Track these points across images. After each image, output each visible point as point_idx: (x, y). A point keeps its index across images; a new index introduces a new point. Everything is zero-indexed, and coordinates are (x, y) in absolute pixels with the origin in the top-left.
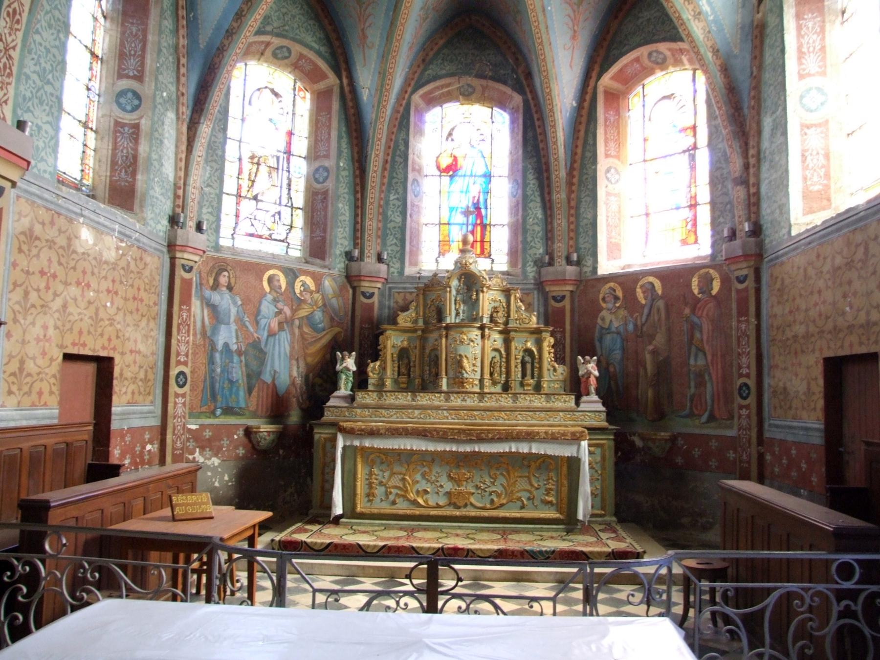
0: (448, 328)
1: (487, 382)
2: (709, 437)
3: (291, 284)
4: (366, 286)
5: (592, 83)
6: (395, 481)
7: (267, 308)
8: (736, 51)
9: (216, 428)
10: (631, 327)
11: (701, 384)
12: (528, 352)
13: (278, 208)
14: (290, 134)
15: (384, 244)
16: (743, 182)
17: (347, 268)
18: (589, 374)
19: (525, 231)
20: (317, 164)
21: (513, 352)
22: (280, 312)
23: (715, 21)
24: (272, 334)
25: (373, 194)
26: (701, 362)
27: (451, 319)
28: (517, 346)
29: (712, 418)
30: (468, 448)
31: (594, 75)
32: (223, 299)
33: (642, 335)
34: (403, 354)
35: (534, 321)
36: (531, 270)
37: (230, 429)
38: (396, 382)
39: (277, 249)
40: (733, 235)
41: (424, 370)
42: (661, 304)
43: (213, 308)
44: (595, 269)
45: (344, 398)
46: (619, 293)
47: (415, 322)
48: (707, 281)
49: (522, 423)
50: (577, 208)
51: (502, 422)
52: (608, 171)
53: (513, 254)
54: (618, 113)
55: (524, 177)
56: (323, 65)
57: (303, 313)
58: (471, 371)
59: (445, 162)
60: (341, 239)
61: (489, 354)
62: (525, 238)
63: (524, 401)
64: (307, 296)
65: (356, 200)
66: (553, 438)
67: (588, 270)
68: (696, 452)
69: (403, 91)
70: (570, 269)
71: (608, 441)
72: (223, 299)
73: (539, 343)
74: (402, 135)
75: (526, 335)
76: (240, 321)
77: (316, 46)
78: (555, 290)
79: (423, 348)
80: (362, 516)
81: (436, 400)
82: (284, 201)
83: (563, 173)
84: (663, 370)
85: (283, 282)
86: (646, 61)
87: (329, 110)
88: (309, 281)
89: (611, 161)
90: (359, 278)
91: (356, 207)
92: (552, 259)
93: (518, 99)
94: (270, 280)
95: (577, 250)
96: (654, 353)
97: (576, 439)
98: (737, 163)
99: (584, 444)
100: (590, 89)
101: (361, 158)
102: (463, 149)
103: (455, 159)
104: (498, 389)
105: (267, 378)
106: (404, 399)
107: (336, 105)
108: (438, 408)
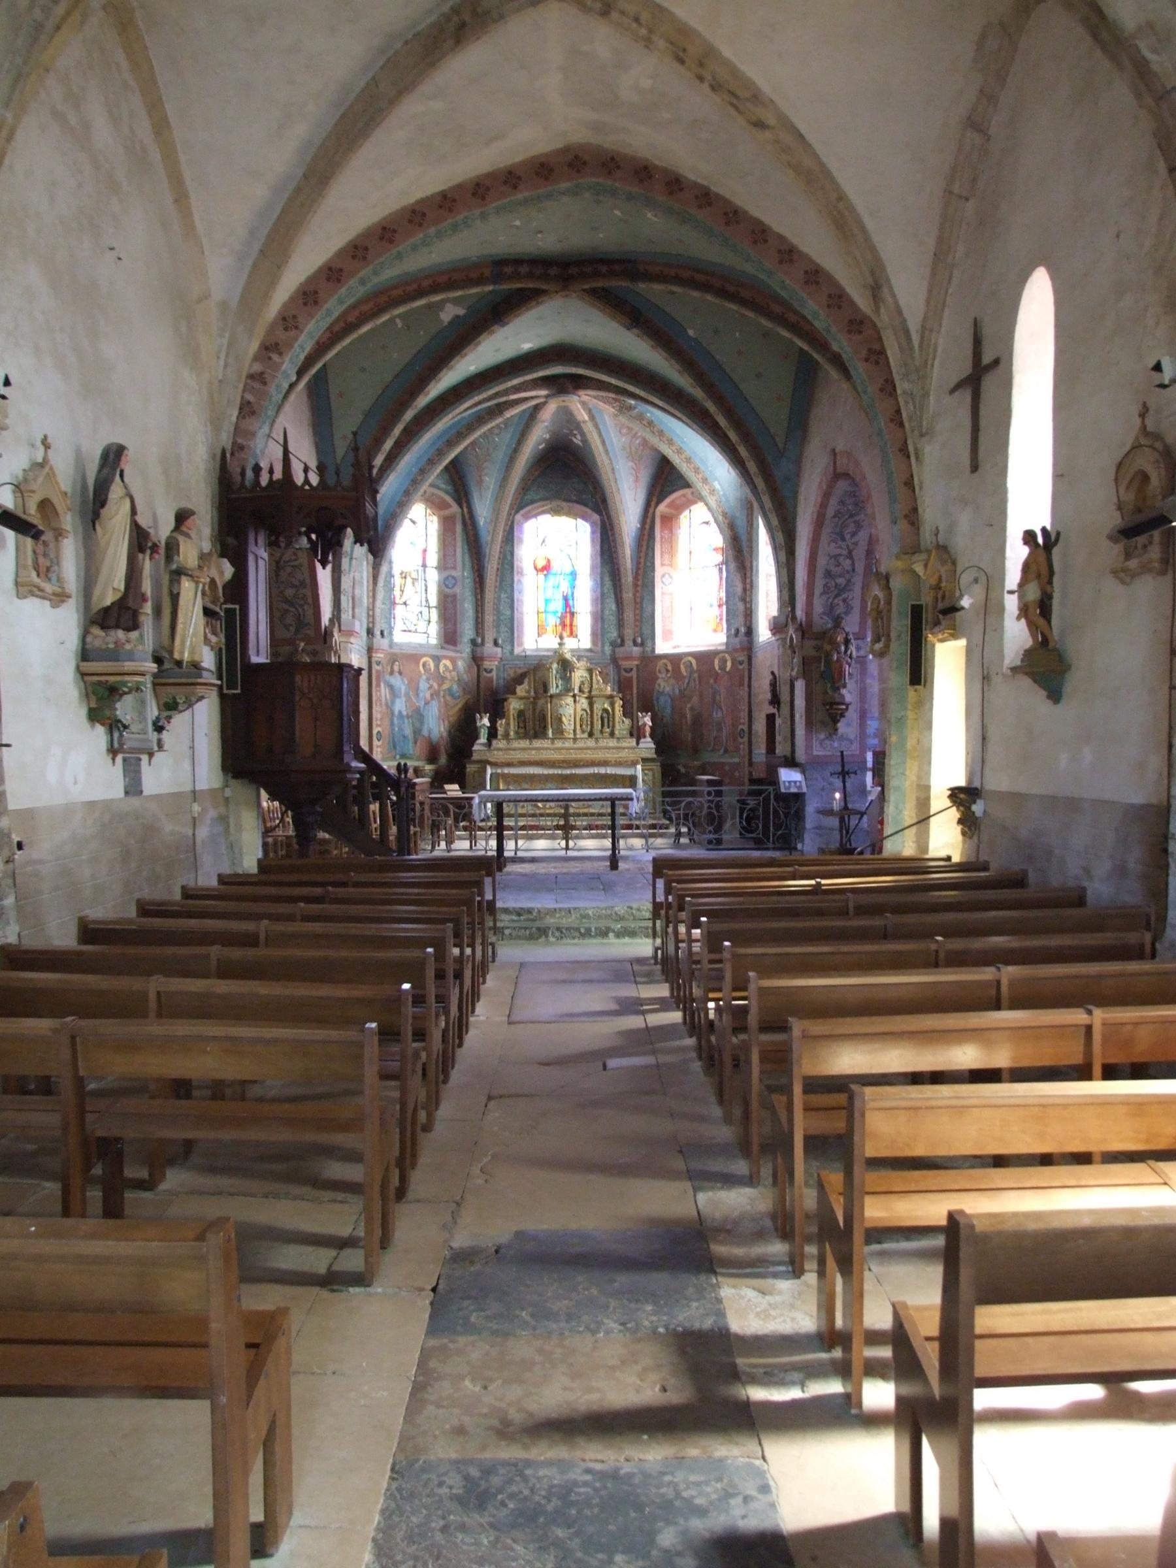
0: (551, 696)
1: (578, 731)
3: (437, 666)
4: (487, 664)
5: (651, 510)
7: (423, 685)
8: (738, 515)
10: (677, 691)
11: (720, 730)
12: (605, 710)
13: (420, 609)
14: (425, 551)
15: (498, 632)
16: (744, 600)
17: (473, 651)
18: (645, 724)
19: (603, 620)
20: (447, 573)
21: (595, 711)
22: (431, 687)
23: (724, 495)
24: (427, 703)
25: (489, 595)
26: (720, 715)
27: (553, 690)
28: (598, 707)
29: (726, 751)
30: (568, 772)
31: (653, 504)
32: (396, 681)
33: (684, 696)
34: (521, 714)
35: (609, 690)
36: (608, 649)
38: (517, 733)
39: (419, 639)
40: (737, 631)
41: (536, 724)
42: (696, 675)
43: (391, 687)
44: (653, 650)
45: (483, 744)
46: (670, 668)
47: (528, 692)
48: (724, 661)
49: (600, 755)
50: (641, 603)
51: (589, 756)
52: (663, 576)
53: (594, 634)
54: (671, 531)
55: (602, 578)
56: (448, 499)
57: (445, 687)
58: (568, 725)
59: (540, 565)
60: (467, 630)
61: (579, 712)
62: (603, 625)
63: (603, 743)
64: (448, 675)
65: (477, 600)
66: (619, 764)
67: (649, 649)
69: (509, 514)
70: (636, 649)
71: (656, 767)
72: (396, 681)
73: (612, 705)
74: (509, 548)
75: (603, 699)
77: (443, 486)
78: (625, 664)
79: (534, 710)
81: (545, 743)
82: (424, 603)
83: (630, 579)
84: (698, 720)
85: (432, 665)
86: (690, 497)
87: (454, 533)
88: (448, 663)
89: (666, 569)
90: (482, 659)
91: (477, 605)
92: (623, 641)
93: (596, 517)
94: (424, 665)
95: (641, 635)
96: (692, 709)
97: (634, 764)
98: (739, 588)
99: (639, 767)
100: (650, 515)
101: (480, 570)
102: (554, 551)
103: (549, 561)
104: (586, 735)
105: (425, 733)
106: (524, 743)
107: (459, 528)
108: (547, 749)
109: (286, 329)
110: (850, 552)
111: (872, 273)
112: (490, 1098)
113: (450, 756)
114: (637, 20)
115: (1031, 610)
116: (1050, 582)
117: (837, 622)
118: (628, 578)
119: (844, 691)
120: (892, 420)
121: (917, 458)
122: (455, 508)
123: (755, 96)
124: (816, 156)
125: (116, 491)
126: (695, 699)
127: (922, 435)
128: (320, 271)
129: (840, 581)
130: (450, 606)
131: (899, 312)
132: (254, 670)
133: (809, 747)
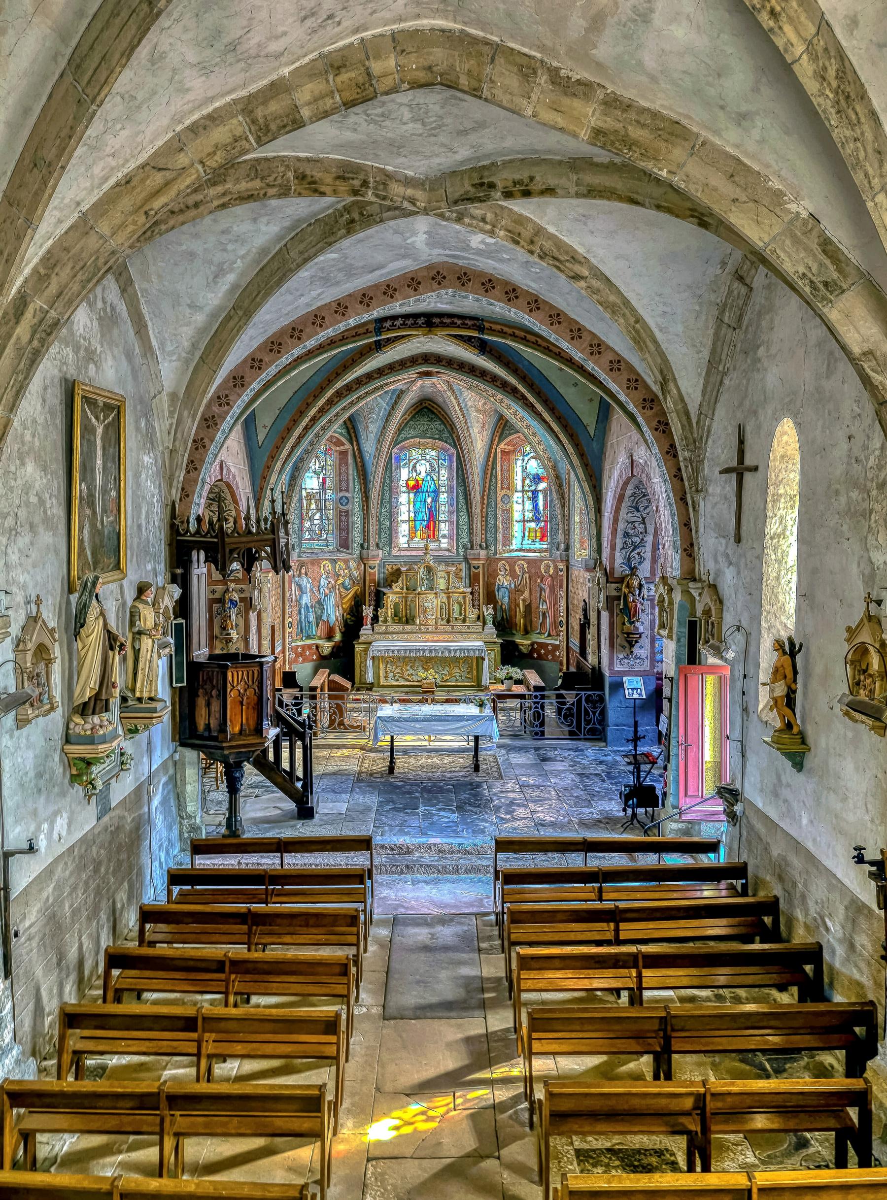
2: (548, 644)
3: (334, 568)
4: (371, 563)
6: (398, 670)
9: (303, 647)
12: (459, 603)
25: (373, 511)
29: (549, 635)
34: (396, 605)
37: (309, 647)
43: (300, 586)
57: (339, 582)
59: (412, 483)
68: (543, 652)
72: (305, 582)
76: (311, 590)
78: (474, 563)
80: (383, 687)
83: (477, 488)
93: (452, 450)
96: (524, 600)
107: (351, 461)
109: (220, 405)
110: (644, 519)
111: (661, 372)
112: (368, 1160)
113: (343, 634)
114: (483, 220)
115: (779, 702)
116: (795, 681)
117: (633, 570)
118: (476, 498)
119: (638, 624)
120: (675, 476)
121: (694, 508)
122: (348, 446)
123: (573, 258)
124: (619, 293)
125: (93, 612)
126: (526, 594)
127: (697, 491)
128: (245, 361)
129: (634, 539)
130: (343, 518)
131: (682, 399)
132: (194, 668)
133: (611, 663)
